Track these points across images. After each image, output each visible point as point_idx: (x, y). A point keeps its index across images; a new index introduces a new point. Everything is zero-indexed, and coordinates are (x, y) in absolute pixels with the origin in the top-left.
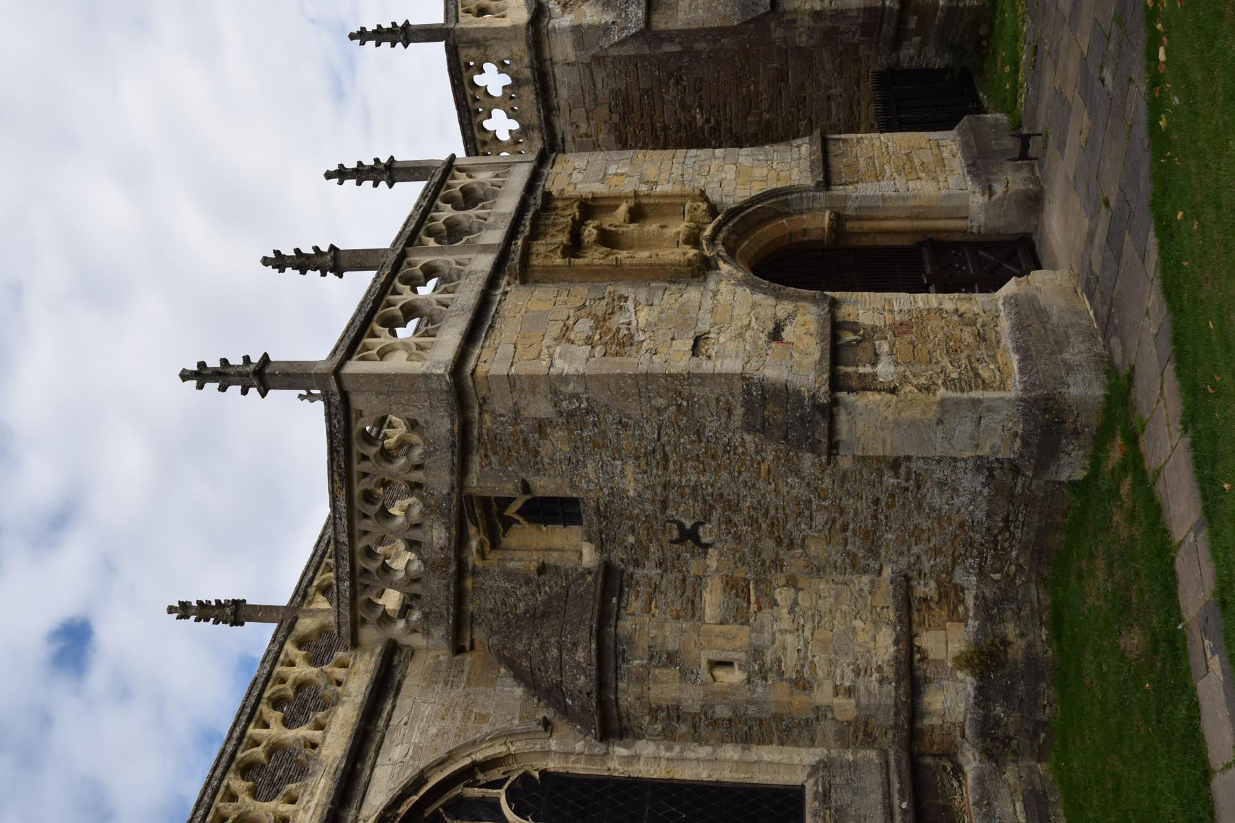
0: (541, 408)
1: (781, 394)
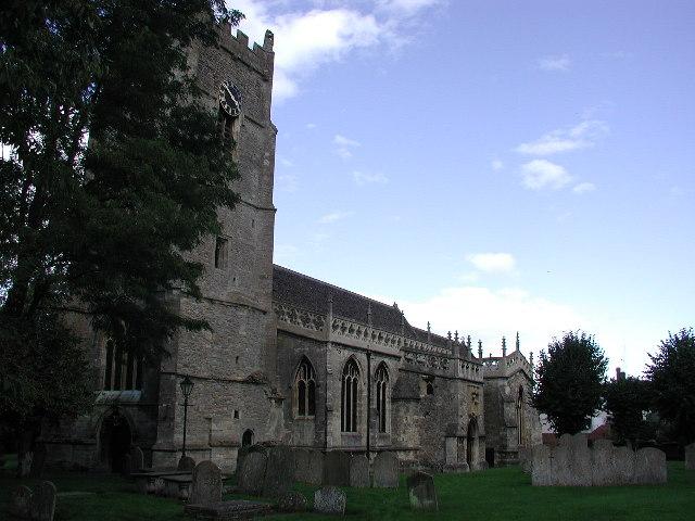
0: (452, 391)
1: (456, 429)
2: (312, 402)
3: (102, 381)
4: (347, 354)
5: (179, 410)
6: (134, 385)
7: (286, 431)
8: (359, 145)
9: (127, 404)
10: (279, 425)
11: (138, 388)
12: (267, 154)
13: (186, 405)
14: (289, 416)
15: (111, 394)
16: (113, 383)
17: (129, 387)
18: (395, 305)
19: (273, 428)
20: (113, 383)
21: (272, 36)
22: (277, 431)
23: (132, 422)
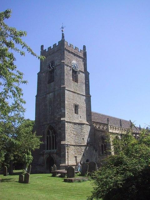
2: (56, 146)
3: (46, 148)
4: (114, 136)
5: (67, 154)
6: (49, 149)
7: (98, 159)
8: (62, 86)
9: (53, 153)
10: (96, 158)
11: (56, 149)
12: (87, 80)
13: (68, 152)
14: (99, 155)
15: (49, 151)
16: (55, 148)
17: (53, 149)
18: (130, 121)
19: (95, 158)
20: (55, 148)
21: (85, 47)
22: (96, 159)
23: (55, 159)
